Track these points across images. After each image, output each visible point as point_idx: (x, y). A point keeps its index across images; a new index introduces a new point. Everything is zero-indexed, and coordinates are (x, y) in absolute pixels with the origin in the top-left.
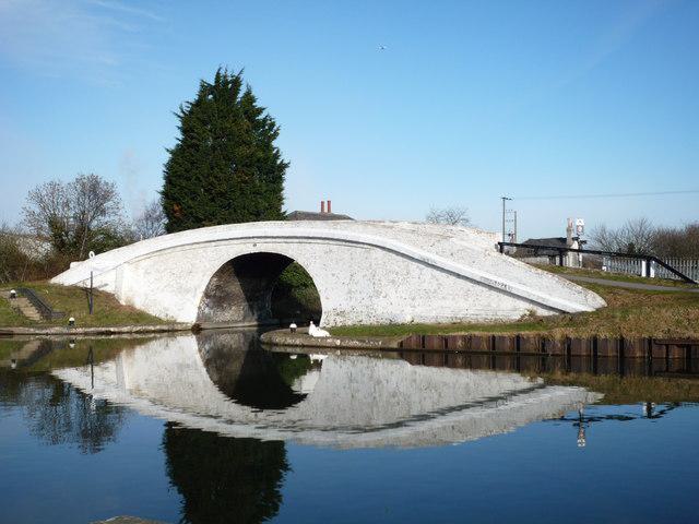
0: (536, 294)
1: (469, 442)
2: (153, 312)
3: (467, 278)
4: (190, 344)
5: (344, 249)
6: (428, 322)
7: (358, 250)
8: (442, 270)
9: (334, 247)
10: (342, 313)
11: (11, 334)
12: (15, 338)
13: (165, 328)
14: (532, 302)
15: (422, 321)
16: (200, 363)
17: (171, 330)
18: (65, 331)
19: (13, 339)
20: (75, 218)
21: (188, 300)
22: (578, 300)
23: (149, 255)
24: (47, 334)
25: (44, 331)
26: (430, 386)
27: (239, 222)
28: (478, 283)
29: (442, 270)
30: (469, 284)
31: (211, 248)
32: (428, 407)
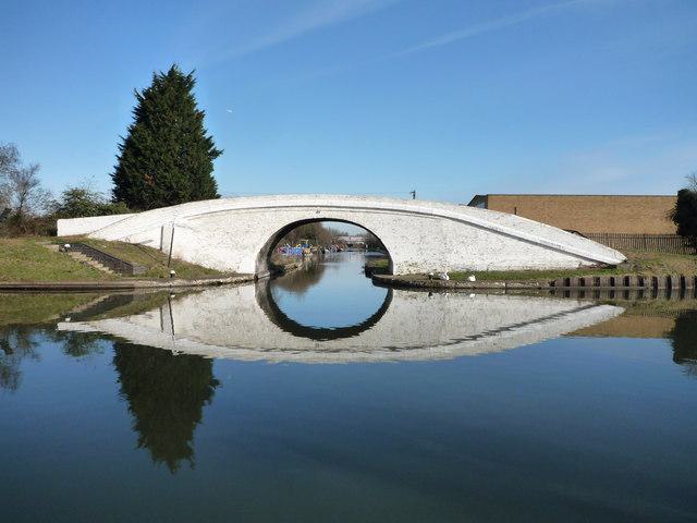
1: (521, 347)
2: (207, 264)
5: (416, 220)
6: (516, 269)
7: (428, 220)
9: (404, 217)
15: (413, 271)
16: (255, 302)
17: (216, 280)
18: (186, 283)
22: (613, 257)
23: (197, 217)
24: (171, 287)
26: (494, 312)
27: (197, 200)
28: (536, 244)
30: (529, 245)
31: (269, 214)
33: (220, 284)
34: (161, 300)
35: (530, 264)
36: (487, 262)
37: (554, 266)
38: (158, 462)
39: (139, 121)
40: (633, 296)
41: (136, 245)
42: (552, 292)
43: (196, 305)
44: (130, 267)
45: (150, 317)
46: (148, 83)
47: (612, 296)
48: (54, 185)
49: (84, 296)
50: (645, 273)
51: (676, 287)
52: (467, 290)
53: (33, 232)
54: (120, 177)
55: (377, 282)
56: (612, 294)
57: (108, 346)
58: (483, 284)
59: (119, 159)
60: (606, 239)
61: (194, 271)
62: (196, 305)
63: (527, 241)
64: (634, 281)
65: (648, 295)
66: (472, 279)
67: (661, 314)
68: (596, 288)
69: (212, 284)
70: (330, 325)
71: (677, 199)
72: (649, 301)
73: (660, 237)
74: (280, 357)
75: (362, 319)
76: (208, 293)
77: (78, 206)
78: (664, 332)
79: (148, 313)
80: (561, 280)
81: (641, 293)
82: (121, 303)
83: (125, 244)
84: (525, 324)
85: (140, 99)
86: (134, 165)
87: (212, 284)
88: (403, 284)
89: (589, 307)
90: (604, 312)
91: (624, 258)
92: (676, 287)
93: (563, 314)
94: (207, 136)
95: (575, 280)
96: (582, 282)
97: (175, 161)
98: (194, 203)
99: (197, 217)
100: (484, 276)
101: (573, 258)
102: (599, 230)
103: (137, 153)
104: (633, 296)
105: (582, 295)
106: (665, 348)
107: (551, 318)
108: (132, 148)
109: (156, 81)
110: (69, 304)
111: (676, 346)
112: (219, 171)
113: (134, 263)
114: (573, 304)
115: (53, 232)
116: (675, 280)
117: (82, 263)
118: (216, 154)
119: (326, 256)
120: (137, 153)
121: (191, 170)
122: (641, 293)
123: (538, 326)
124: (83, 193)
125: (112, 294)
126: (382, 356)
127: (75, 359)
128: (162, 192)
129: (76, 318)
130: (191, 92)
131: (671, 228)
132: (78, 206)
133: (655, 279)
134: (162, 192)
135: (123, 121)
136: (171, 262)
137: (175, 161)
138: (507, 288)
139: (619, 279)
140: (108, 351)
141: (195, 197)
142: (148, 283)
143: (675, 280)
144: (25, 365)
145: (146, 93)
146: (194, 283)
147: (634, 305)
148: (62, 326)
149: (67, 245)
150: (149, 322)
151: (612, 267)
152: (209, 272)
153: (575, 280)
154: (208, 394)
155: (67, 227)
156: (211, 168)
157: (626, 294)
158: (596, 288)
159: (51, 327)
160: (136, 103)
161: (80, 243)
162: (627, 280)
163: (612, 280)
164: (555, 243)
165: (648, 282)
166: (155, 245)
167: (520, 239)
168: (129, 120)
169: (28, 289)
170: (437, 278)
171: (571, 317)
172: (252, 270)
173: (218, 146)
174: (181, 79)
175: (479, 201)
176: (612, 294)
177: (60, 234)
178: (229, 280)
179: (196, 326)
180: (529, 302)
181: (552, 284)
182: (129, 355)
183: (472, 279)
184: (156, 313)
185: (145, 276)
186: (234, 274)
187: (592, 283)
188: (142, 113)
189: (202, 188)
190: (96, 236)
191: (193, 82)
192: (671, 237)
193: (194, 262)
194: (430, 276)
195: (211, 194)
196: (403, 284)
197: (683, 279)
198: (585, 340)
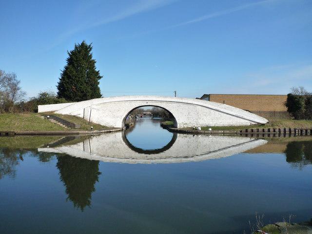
2: (102, 124)
3: (230, 114)
5: (187, 106)
7: (191, 106)
8: (221, 112)
9: (181, 105)
10: (186, 124)
12: (80, 135)
13: (118, 130)
14: (250, 120)
15: (186, 126)
17: (109, 130)
18: (99, 132)
22: (263, 121)
23: (98, 105)
24: (93, 133)
28: (234, 116)
29: (221, 112)
30: (231, 116)
31: (127, 104)
32: (217, 149)
33: (110, 132)
34: (83, 139)
35: (231, 124)
36: (215, 123)
37: (241, 124)
38: (76, 208)
39: (69, 64)
40: (272, 136)
41: (74, 116)
42: (241, 135)
43: (98, 141)
44: (74, 125)
45: (79, 145)
46: (73, 49)
47: (263, 136)
48: (29, 91)
51: (287, 132)
52: (207, 134)
53: (28, 111)
54: (61, 87)
55: (170, 131)
56: (263, 135)
57: (55, 157)
58: (215, 132)
59: (60, 79)
60: (260, 113)
62: (98, 141)
64: (272, 130)
65: (277, 135)
66: (210, 129)
67: (281, 143)
68: (274, 133)
69: (108, 132)
70: (144, 148)
71: (287, 97)
72: (277, 138)
73: (280, 113)
74: (131, 161)
75: (161, 147)
76: (103, 136)
77: (44, 99)
78: (282, 151)
79: (78, 144)
80: (244, 130)
81: (274, 135)
82: (70, 140)
83: (70, 116)
84: (229, 147)
85: (70, 55)
87: (108, 132)
88: (182, 132)
90: (261, 142)
91: (268, 121)
92: (287, 132)
93: (244, 143)
95: (249, 130)
96: (252, 130)
97: (85, 81)
99: (98, 105)
100: (214, 128)
104: (272, 136)
105: (252, 136)
106: (283, 157)
107: (239, 145)
109: (76, 47)
110: (50, 140)
111: (287, 156)
112: (102, 85)
113: (76, 124)
114: (248, 139)
115: (36, 111)
116: (287, 130)
118: (100, 78)
119: (137, 120)
120: (69, 77)
121: (91, 85)
122: (274, 135)
124: (47, 94)
126: (173, 161)
127: (44, 163)
128: (79, 94)
129: (52, 146)
130: (91, 52)
131: (286, 109)
133: (280, 129)
134: (79, 94)
136: (90, 123)
137: (85, 81)
138: (224, 133)
139: (266, 129)
140: (55, 161)
141: (98, 98)
142: (84, 132)
143: (287, 130)
144: (17, 167)
145: (72, 52)
146: (101, 131)
147: (272, 139)
148: (40, 150)
149: (48, 117)
150: (79, 147)
151: (263, 125)
152: (104, 127)
153: (249, 130)
154: (96, 178)
155: (42, 109)
156: (98, 83)
157: (269, 135)
159: (35, 151)
160: (68, 56)
161: (52, 115)
162: (269, 129)
163: (264, 130)
164: (241, 115)
165: (277, 130)
166: (81, 116)
167: (227, 114)
168: (65, 64)
170: (196, 129)
171: (247, 144)
172: (121, 126)
173: (101, 75)
174: (86, 46)
175: (206, 97)
176: (263, 135)
178: (113, 130)
179: (97, 149)
181: (241, 131)
182: (65, 161)
183: (210, 129)
184: (81, 144)
185: (80, 129)
186: (114, 128)
187: (256, 131)
188: (70, 61)
189: (95, 94)
192: (284, 113)
193: (97, 123)
195: (99, 96)
196: (182, 132)
197: (290, 129)
198: (248, 154)
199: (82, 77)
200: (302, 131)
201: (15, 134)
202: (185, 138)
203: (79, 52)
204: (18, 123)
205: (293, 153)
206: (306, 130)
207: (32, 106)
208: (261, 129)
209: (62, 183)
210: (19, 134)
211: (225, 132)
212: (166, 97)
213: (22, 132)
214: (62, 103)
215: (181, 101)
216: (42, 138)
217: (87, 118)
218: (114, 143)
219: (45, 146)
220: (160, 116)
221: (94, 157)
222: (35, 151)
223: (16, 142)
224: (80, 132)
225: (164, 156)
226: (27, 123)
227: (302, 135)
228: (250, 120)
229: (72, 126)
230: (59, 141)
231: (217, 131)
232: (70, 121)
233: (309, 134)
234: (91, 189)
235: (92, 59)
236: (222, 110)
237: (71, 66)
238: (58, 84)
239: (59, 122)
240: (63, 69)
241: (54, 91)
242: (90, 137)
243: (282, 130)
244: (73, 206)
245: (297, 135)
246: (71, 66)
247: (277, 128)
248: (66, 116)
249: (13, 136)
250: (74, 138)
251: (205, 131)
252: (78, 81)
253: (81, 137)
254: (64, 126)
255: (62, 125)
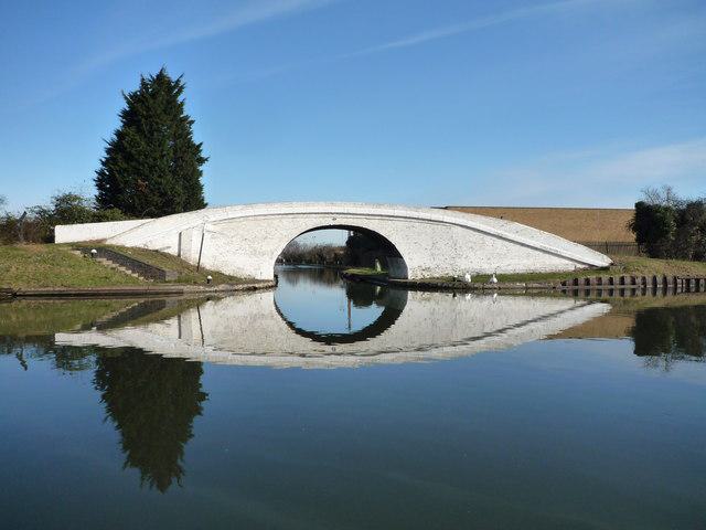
0: (577, 257)
2: (227, 271)
4: (413, 274)
11: (180, 293)
12: (185, 296)
14: (572, 260)
15: (427, 275)
17: (252, 287)
19: (182, 298)
20: (656, 366)
21: (32, 211)
22: (602, 260)
23: (215, 223)
24: (216, 291)
25: (212, 289)
28: (536, 249)
31: (286, 221)
33: (255, 289)
34: (180, 310)
39: (125, 125)
46: (135, 87)
47: (600, 295)
48: (25, 198)
49: (114, 302)
50: (637, 273)
61: (219, 277)
63: (528, 246)
65: (639, 292)
66: (495, 280)
68: (633, 287)
74: (297, 361)
76: (228, 301)
77: (69, 212)
79: (166, 321)
82: (150, 309)
83: (143, 250)
86: (125, 170)
89: (582, 306)
90: (600, 308)
91: (610, 261)
94: (115, 137)
95: (582, 280)
96: (588, 282)
98: (187, 214)
100: (502, 278)
101: (567, 262)
102: (586, 239)
103: (128, 158)
105: (575, 294)
106: (629, 345)
108: (119, 152)
109: (144, 84)
110: (103, 310)
112: (208, 179)
114: (571, 302)
115: (50, 239)
117: (112, 268)
120: (128, 158)
122: (634, 290)
123: (539, 325)
124: (76, 198)
125: (142, 301)
128: (156, 198)
131: (632, 237)
132: (69, 212)
134: (156, 198)
135: (110, 124)
138: (527, 288)
140: (88, 373)
141: (199, 208)
142: (195, 288)
146: (236, 287)
148: (62, 338)
149: (94, 251)
151: (605, 269)
152: (231, 279)
155: (65, 234)
156: (200, 174)
158: (633, 287)
159: (46, 343)
162: (622, 278)
164: (553, 248)
165: (639, 281)
166: (173, 251)
167: (523, 245)
168: (118, 124)
169: (75, 295)
171: (568, 315)
174: (169, 82)
177: (58, 240)
178: (261, 285)
180: (532, 301)
184: (174, 322)
185: (179, 281)
187: (571, 281)
188: (129, 117)
189: (193, 201)
190: (114, 242)
191: (182, 88)
194: (454, 279)
197: (665, 278)
199: (163, 156)
200: (688, 281)
201: (15, 295)
202: (428, 303)
203: (153, 96)
204: (18, 267)
205: (651, 334)
206: (698, 281)
207: (39, 229)
208: (605, 277)
209: (111, 425)
210: (25, 296)
211: (530, 286)
212: (379, 205)
213: (32, 289)
214: (113, 220)
215: (415, 215)
216: (84, 308)
217: (192, 258)
218: (254, 318)
219: (86, 328)
220: (309, 262)
221: (192, 352)
222: (46, 343)
223: (14, 319)
224: (186, 288)
225: (376, 348)
226: (42, 267)
227: (688, 290)
228: (572, 260)
229: (158, 275)
230: (122, 314)
231: (510, 284)
232: (140, 258)
233: (702, 289)
234: (184, 433)
235: (185, 114)
236: (511, 236)
237: (133, 129)
238: (97, 175)
239: (122, 265)
240: (111, 136)
241: (89, 193)
242: (198, 304)
243: (649, 281)
244: (122, 465)
245: (679, 290)
246: (133, 129)
247: (640, 275)
248: (135, 250)
249: (9, 300)
250: (162, 305)
251: (480, 285)
252: (151, 168)
253: (188, 301)
254: (136, 275)
255: (129, 272)
